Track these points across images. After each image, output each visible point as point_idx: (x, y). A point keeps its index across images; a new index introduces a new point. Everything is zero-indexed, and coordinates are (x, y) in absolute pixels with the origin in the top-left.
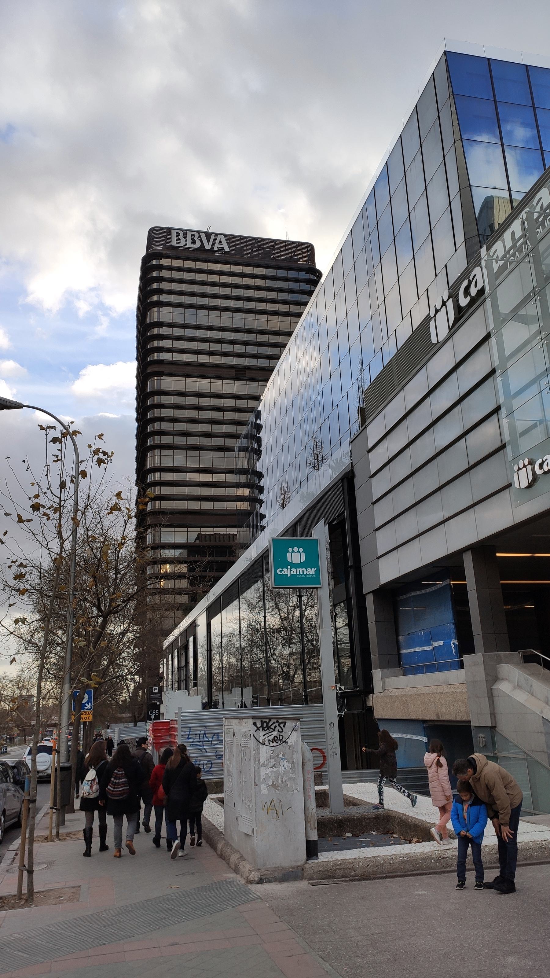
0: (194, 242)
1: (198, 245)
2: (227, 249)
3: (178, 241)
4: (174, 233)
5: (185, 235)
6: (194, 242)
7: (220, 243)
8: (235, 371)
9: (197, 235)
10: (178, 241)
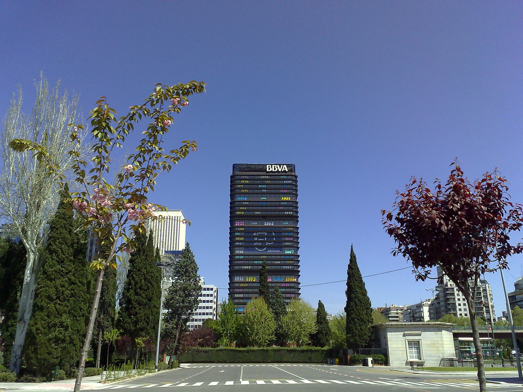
0: (275, 169)
1: (276, 170)
2: (287, 170)
3: (269, 169)
4: (268, 166)
5: (272, 167)
6: (275, 169)
10: (269, 169)
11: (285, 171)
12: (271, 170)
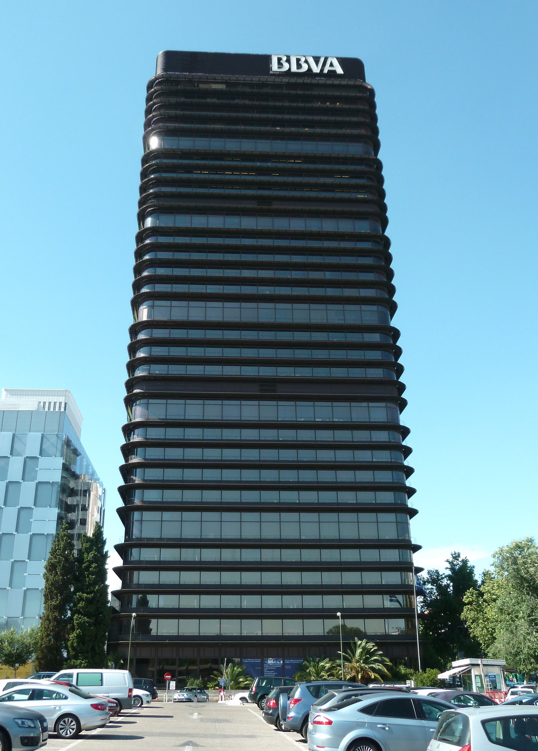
0: (299, 66)
1: (305, 68)
2: (340, 70)
5: (288, 61)
6: (299, 66)
7: (331, 65)
8: (407, 567)
9: (303, 59)
10: (280, 64)
11: (332, 73)
12: (286, 67)
